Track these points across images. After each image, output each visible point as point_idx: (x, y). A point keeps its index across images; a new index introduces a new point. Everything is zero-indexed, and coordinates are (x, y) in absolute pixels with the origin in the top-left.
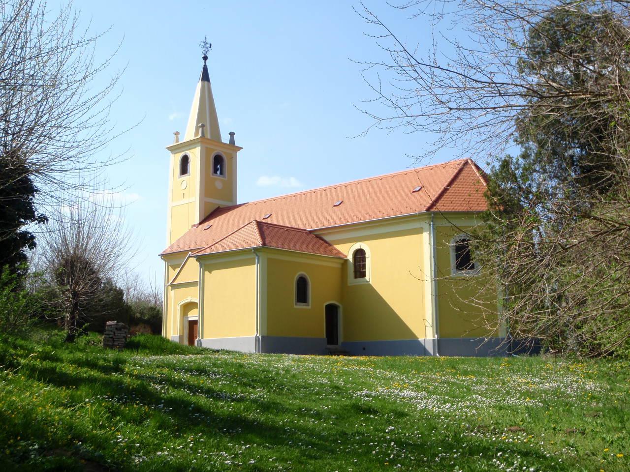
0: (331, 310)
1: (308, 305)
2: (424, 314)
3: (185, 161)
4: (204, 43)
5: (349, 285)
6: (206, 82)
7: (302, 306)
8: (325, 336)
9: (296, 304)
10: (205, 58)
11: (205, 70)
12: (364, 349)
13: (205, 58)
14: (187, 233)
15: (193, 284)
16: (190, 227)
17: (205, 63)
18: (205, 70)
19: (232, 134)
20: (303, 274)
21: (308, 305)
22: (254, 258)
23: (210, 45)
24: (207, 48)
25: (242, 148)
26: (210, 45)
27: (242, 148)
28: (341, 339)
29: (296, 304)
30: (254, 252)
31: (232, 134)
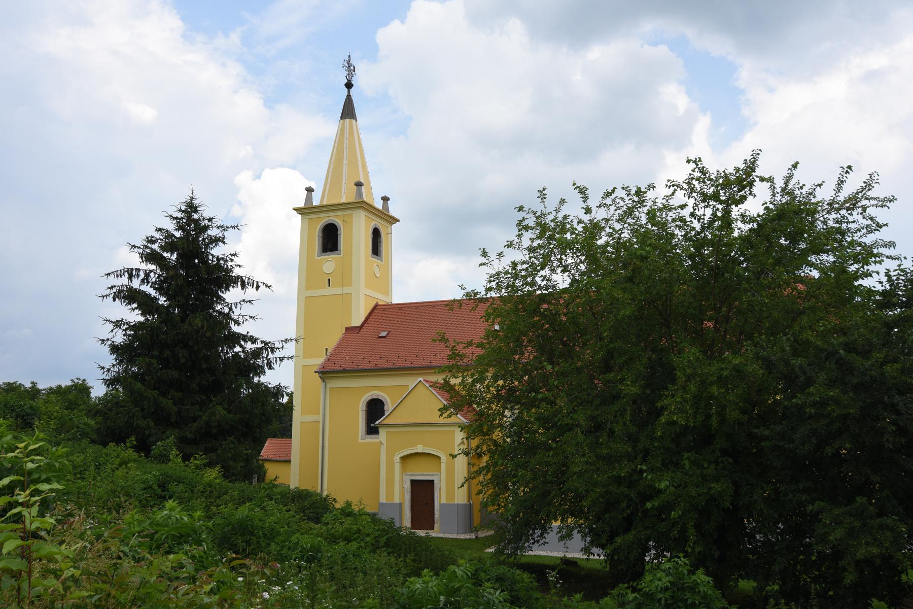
10: (349, 85)
13: (349, 85)
16: (344, 331)
17: (349, 92)
19: (385, 199)
25: (397, 221)
27: (397, 221)
31: (385, 199)
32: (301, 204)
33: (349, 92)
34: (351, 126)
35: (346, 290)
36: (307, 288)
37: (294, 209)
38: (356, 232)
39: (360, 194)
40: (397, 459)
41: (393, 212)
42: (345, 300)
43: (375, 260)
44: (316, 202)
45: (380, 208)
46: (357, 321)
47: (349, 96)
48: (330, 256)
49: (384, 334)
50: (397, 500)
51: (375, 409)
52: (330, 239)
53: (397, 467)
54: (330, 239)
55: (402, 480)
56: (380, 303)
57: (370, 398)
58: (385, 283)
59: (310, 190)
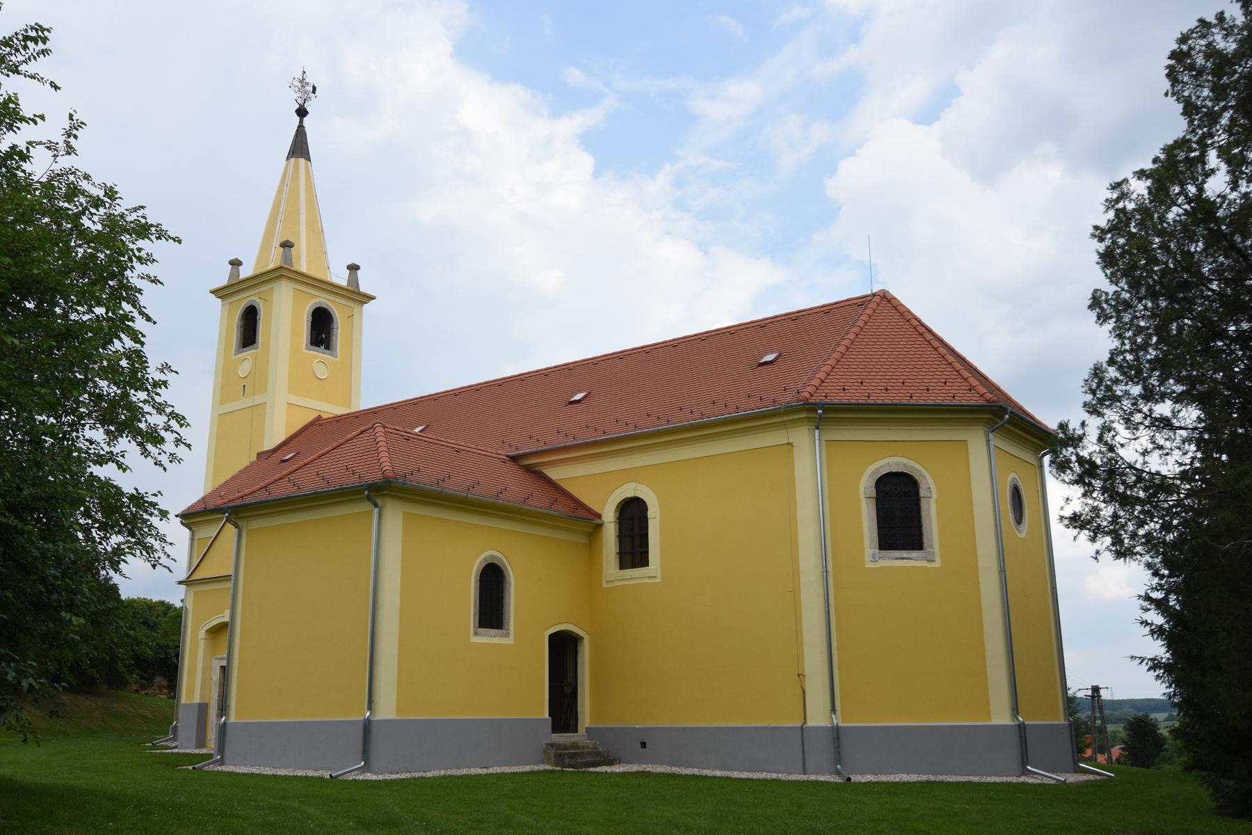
0: (563, 648)
1: (507, 635)
2: (799, 658)
3: (250, 318)
4: (301, 82)
5: (123, 597)
6: (302, 161)
7: (490, 638)
8: (546, 714)
9: (476, 634)
10: (302, 112)
11: (301, 133)
12: (644, 745)
13: (302, 112)
14: (246, 468)
15: (226, 578)
16: (254, 458)
17: (301, 122)
18: (301, 133)
19: (353, 268)
20: (494, 557)
21: (507, 635)
22: (371, 513)
23: (314, 88)
24: (305, 92)
25: (373, 298)
26: (314, 88)
27: (373, 298)
28: (586, 718)
29: (476, 634)
30: (369, 498)
31: (353, 268)
32: (224, 281)
33: (301, 122)
34: (296, 169)
35: (258, 399)
36: (222, 402)
37: (212, 292)
38: (285, 316)
39: (287, 258)
40: (202, 634)
41: (364, 288)
42: (258, 411)
43: (319, 354)
44: (245, 272)
45: (344, 283)
46: (269, 445)
47: (301, 128)
48: (249, 353)
49: (578, 397)
50: (197, 700)
51: (492, 581)
52: (249, 328)
53: (202, 644)
54: (249, 328)
55: (207, 669)
56: (324, 416)
57: (630, 495)
58: (346, 379)
59: (236, 263)
